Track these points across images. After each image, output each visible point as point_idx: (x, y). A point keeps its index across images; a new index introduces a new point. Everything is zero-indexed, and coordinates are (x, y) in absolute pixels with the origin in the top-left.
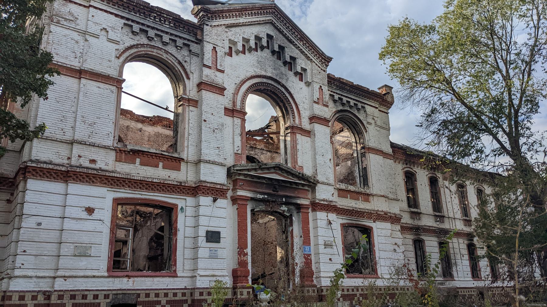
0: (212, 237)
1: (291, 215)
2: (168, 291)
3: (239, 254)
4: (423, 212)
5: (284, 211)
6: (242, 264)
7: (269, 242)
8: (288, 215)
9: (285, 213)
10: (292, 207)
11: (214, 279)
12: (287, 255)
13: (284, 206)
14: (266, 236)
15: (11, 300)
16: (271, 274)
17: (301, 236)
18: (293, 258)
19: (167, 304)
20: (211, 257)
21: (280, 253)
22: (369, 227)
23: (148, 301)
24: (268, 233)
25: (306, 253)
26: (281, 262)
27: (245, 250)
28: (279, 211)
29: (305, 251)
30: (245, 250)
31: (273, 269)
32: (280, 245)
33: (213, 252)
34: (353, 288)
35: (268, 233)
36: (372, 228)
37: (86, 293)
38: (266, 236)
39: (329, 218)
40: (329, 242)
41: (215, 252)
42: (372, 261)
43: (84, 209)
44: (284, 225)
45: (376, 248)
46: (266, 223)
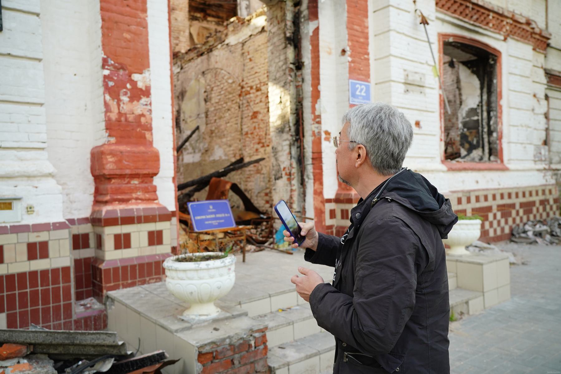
3: (107, 89)
4: (427, 85)
6: (128, 130)
7: (251, 88)
12: (298, 113)
14: (245, 74)
16: (257, 161)
17: (344, 51)
18: (317, 119)
21: (278, 103)
22: (495, 49)
24: (250, 65)
26: (281, 130)
27: (136, 77)
29: (354, 95)
30: (136, 77)
31: (262, 150)
32: (276, 81)
34: (460, 195)
35: (250, 65)
36: (499, 52)
37: (43, 237)
38: (245, 74)
40: (417, 77)
42: (490, 133)
44: (289, 17)
45: (504, 102)
46: (243, 44)
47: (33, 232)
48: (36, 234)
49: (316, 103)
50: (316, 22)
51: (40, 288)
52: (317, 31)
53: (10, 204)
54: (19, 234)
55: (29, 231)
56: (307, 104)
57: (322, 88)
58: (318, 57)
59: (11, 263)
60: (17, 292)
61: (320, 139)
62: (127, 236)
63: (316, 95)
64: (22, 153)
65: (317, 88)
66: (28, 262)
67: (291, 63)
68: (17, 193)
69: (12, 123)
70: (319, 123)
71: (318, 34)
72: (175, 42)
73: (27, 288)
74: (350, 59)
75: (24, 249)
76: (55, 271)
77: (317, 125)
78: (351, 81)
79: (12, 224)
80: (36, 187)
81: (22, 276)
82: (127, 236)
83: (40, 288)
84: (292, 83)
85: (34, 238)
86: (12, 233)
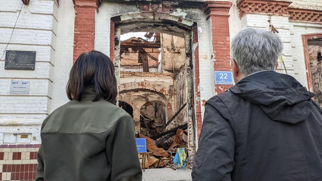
0: (16, 60)
1: (195, 24)
2: (20, 150)
5: (180, 18)
8: (190, 24)
9: (184, 22)
10: (196, 12)
11: (15, 130)
13: (179, 10)
15: (32, 154)
19: (4, 170)
20: (13, 94)
23: (18, 165)
25: (220, 83)
28: (170, 18)
33: (20, 85)
37: (20, 150)
39: (272, 23)
41: (24, 86)
43: (175, 80)
47: (33, 148)
48: (34, 148)
49: (198, 85)
50: (197, 43)
51: (33, 172)
52: (197, 48)
53: (27, 136)
54: (28, 148)
55: (31, 147)
56: (194, 86)
57: (200, 77)
58: (198, 61)
59: (23, 160)
60: (24, 172)
61: (200, 105)
62: (14, 158)
63: (198, 82)
64: (36, 116)
65: (198, 78)
66: (13, 160)
67: (188, 66)
68: (31, 131)
69: (34, 104)
70: (199, 96)
71: (198, 50)
72: (197, 60)
73: (28, 171)
74: (215, 60)
75: (29, 154)
76: (23, 166)
77: (198, 98)
78: (215, 72)
79: (26, 144)
80: (38, 129)
81: (27, 165)
82: (14, 158)
83: (33, 172)
84: (189, 76)
85: (17, 150)
86: (25, 147)
